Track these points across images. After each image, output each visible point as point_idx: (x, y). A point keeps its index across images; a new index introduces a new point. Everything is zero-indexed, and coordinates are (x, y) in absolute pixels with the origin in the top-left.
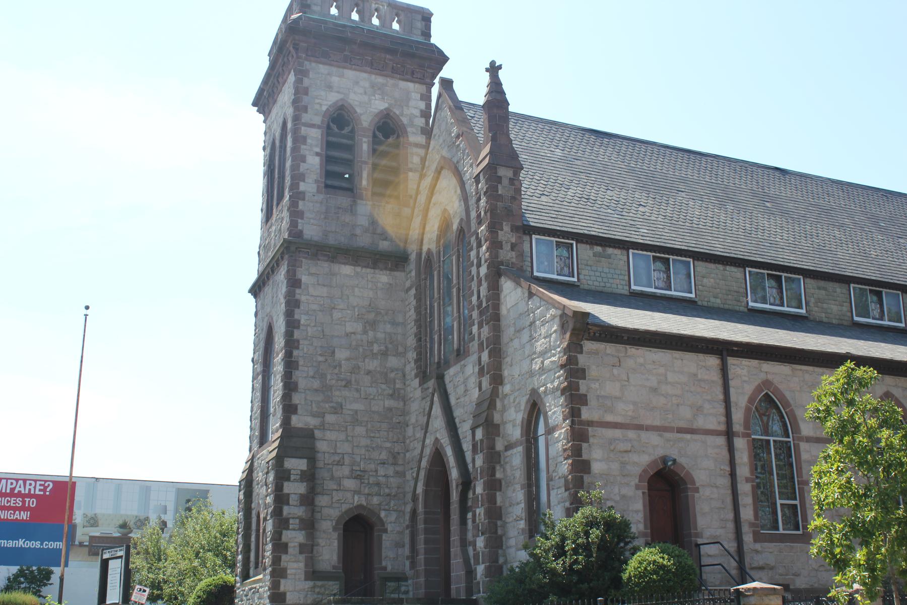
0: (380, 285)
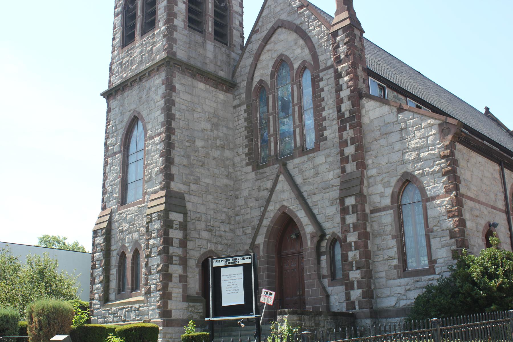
0: (219, 100)
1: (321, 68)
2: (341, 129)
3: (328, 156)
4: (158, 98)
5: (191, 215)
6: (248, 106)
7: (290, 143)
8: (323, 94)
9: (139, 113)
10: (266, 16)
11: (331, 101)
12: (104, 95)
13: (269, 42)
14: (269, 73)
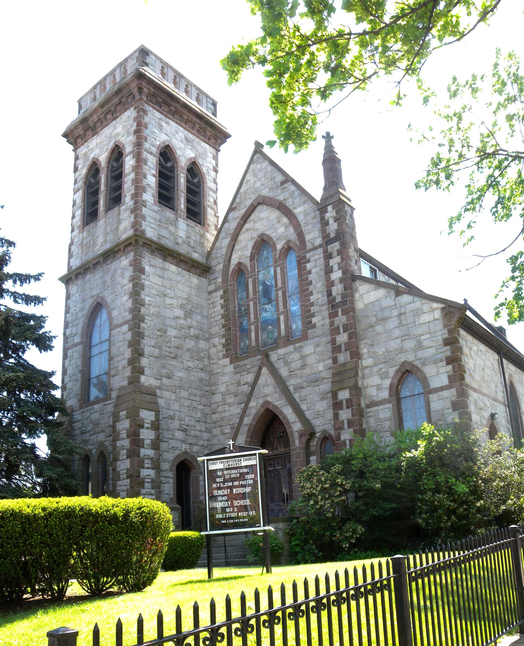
0: (193, 285)
1: (308, 248)
2: (333, 315)
3: (318, 345)
4: (126, 281)
5: (164, 413)
6: (225, 292)
7: (272, 332)
8: (311, 277)
9: (103, 299)
10: (245, 193)
11: (319, 285)
12: (61, 279)
13: (248, 221)
14: (249, 254)
